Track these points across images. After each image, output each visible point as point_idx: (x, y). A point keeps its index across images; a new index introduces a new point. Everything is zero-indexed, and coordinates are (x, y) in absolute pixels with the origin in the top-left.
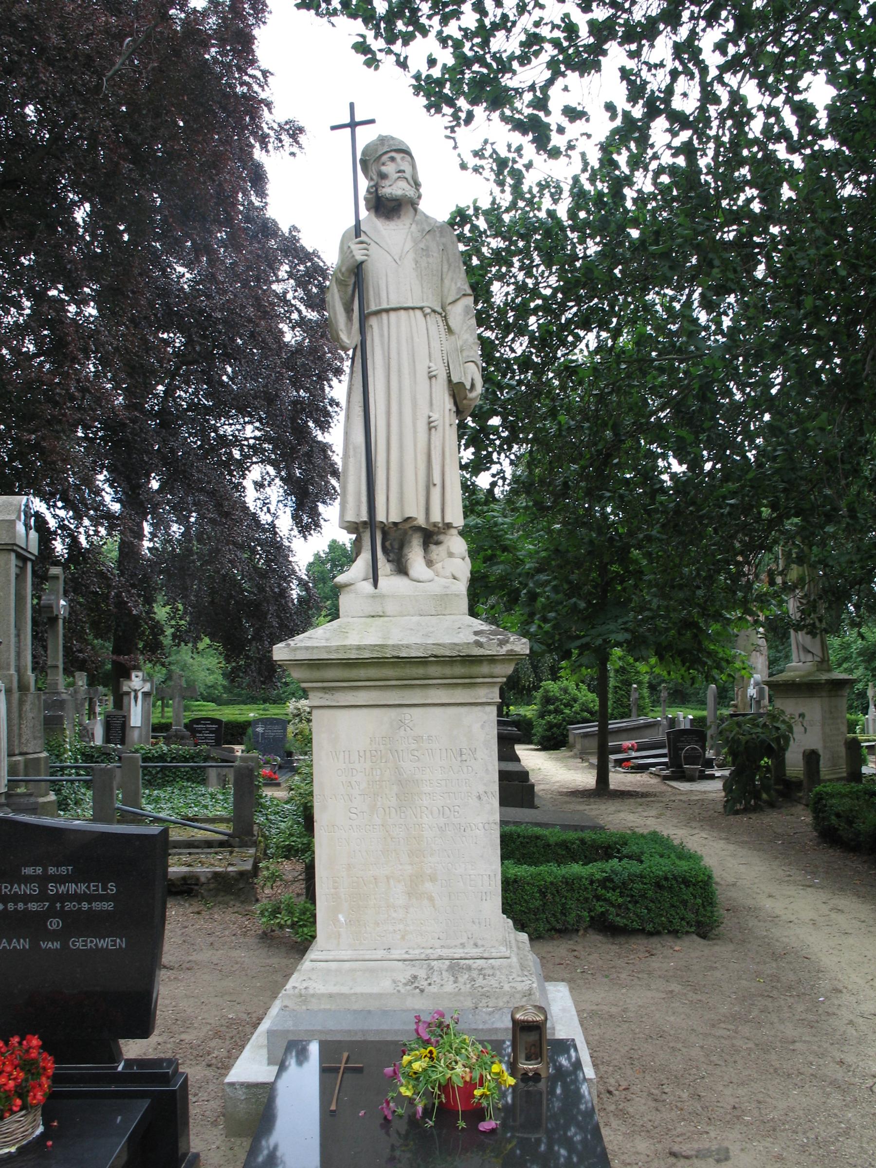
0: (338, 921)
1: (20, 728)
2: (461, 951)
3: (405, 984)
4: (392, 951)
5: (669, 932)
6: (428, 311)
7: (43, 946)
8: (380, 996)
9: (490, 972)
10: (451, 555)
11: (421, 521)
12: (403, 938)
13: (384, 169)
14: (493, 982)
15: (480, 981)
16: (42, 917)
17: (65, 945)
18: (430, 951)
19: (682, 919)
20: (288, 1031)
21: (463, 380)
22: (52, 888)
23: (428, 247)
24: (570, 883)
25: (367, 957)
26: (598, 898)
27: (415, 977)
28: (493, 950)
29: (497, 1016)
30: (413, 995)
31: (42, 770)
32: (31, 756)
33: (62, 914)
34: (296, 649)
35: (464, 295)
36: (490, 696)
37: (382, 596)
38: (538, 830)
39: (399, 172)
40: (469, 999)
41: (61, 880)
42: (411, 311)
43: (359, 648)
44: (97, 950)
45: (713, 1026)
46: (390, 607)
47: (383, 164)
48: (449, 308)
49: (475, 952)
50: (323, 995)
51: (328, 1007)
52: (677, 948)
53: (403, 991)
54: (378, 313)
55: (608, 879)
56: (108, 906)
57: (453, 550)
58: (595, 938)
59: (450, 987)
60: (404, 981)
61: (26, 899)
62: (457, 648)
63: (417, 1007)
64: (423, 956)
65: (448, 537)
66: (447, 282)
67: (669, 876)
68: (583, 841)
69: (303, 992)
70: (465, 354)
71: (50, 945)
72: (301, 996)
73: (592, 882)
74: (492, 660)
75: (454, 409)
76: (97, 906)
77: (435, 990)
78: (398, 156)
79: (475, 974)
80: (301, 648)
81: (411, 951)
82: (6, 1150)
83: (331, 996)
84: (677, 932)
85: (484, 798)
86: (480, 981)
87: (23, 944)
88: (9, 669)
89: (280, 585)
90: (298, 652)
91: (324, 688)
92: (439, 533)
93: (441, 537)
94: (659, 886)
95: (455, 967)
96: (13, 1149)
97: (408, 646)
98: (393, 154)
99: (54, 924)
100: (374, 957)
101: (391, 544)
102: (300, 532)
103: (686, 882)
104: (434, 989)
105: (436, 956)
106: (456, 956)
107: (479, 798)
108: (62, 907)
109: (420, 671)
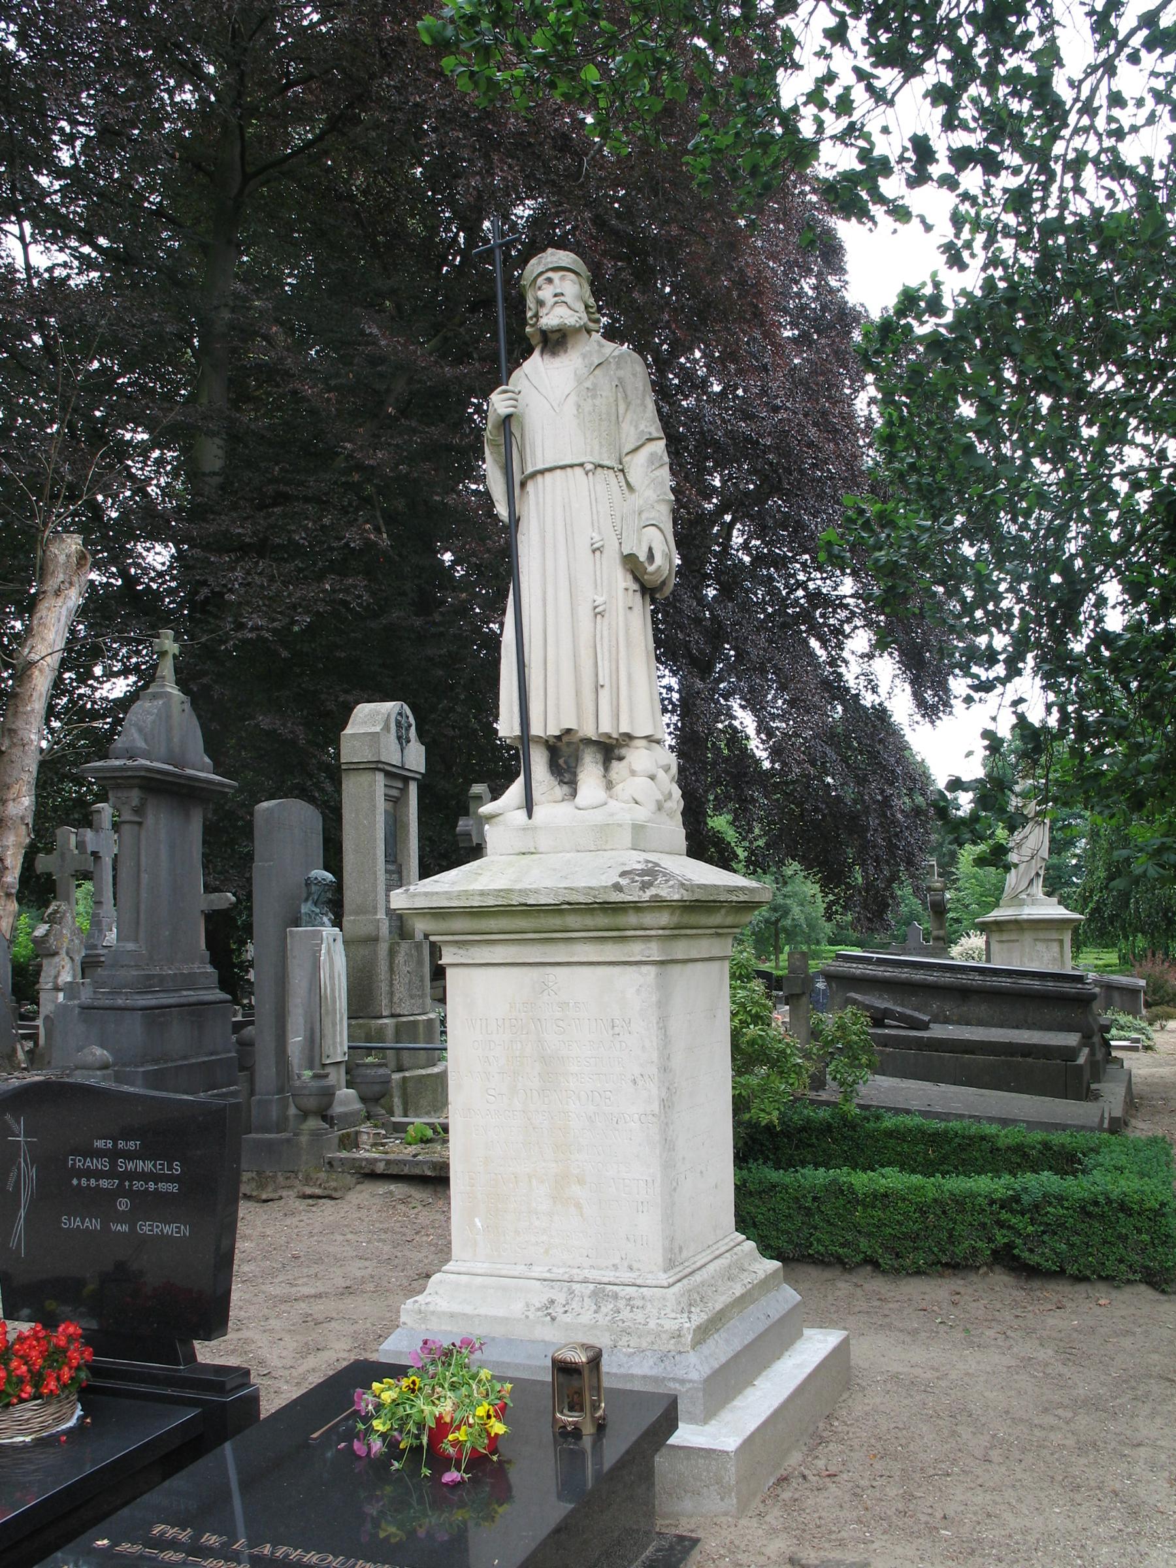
0: (475, 1225)
1: (391, 985)
2: (612, 1273)
3: (538, 1309)
4: (534, 1268)
5: (1100, 1277)
6: (589, 467)
7: (113, 1228)
8: (505, 1320)
9: (640, 1303)
10: (633, 773)
11: (589, 731)
12: (547, 1252)
13: (540, 294)
14: (639, 1316)
15: (626, 1314)
16: (113, 1195)
17: (133, 1228)
18: (578, 1271)
19: (1121, 1261)
20: (401, 1353)
21: (634, 551)
22: (123, 1165)
23: (595, 385)
24: (960, 1202)
25: (503, 1272)
26: (1001, 1224)
27: (552, 1302)
28: (650, 1276)
29: (637, 1359)
30: (543, 1323)
31: (421, 1036)
32: (404, 1019)
33: (131, 1194)
34: (414, 895)
35: (650, 440)
36: (647, 953)
37: (534, 829)
38: (991, 1129)
39: (556, 295)
40: (607, 1334)
41: (129, 1156)
42: (569, 470)
43: (482, 893)
44: (162, 1237)
45: (1046, 1410)
46: (544, 842)
47: (540, 288)
48: (626, 459)
49: (627, 1276)
50: (444, 1313)
51: (449, 1328)
52: (1102, 1302)
53: (531, 1316)
54: (533, 475)
55: (1016, 1199)
56: (173, 1188)
57: (635, 767)
58: (1000, 1279)
59: (587, 1318)
60: (538, 1305)
61: (98, 1174)
62: (593, 893)
63: (547, 1339)
64: (566, 1277)
65: (632, 750)
66: (625, 426)
67: (1101, 1199)
68: (1046, 1145)
69: (423, 1308)
70: (644, 516)
71: (119, 1227)
72: (420, 1312)
73: (992, 1202)
74: (636, 907)
75: (636, 587)
76: (163, 1187)
77: (568, 1320)
78: (555, 276)
79: (621, 1304)
80: (419, 894)
81: (555, 1270)
82: (21, 1439)
83: (452, 1315)
84: (1113, 1278)
85: (640, 1082)
86: (626, 1314)
87: (93, 1224)
88: (375, 913)
89: (882, 791)
90: (417, 899)
91: (456, 942)
92: (621, 746)
93: (623, 751)
94: (1085, 1212)
95: (601, 1293)
96: (28, 1439)
97: (536, 891)
98: (550, 274)
99: (123, 1205)
100: (512, 1273)
101: (566, 762)
102: (923, 716)
103: (1123, 1207)
104: (567, 1318)
105: (580, 1278)
106: (606, 1280)
107: (635, 1082)
108: (131, 1186)
109: (556, 921)
